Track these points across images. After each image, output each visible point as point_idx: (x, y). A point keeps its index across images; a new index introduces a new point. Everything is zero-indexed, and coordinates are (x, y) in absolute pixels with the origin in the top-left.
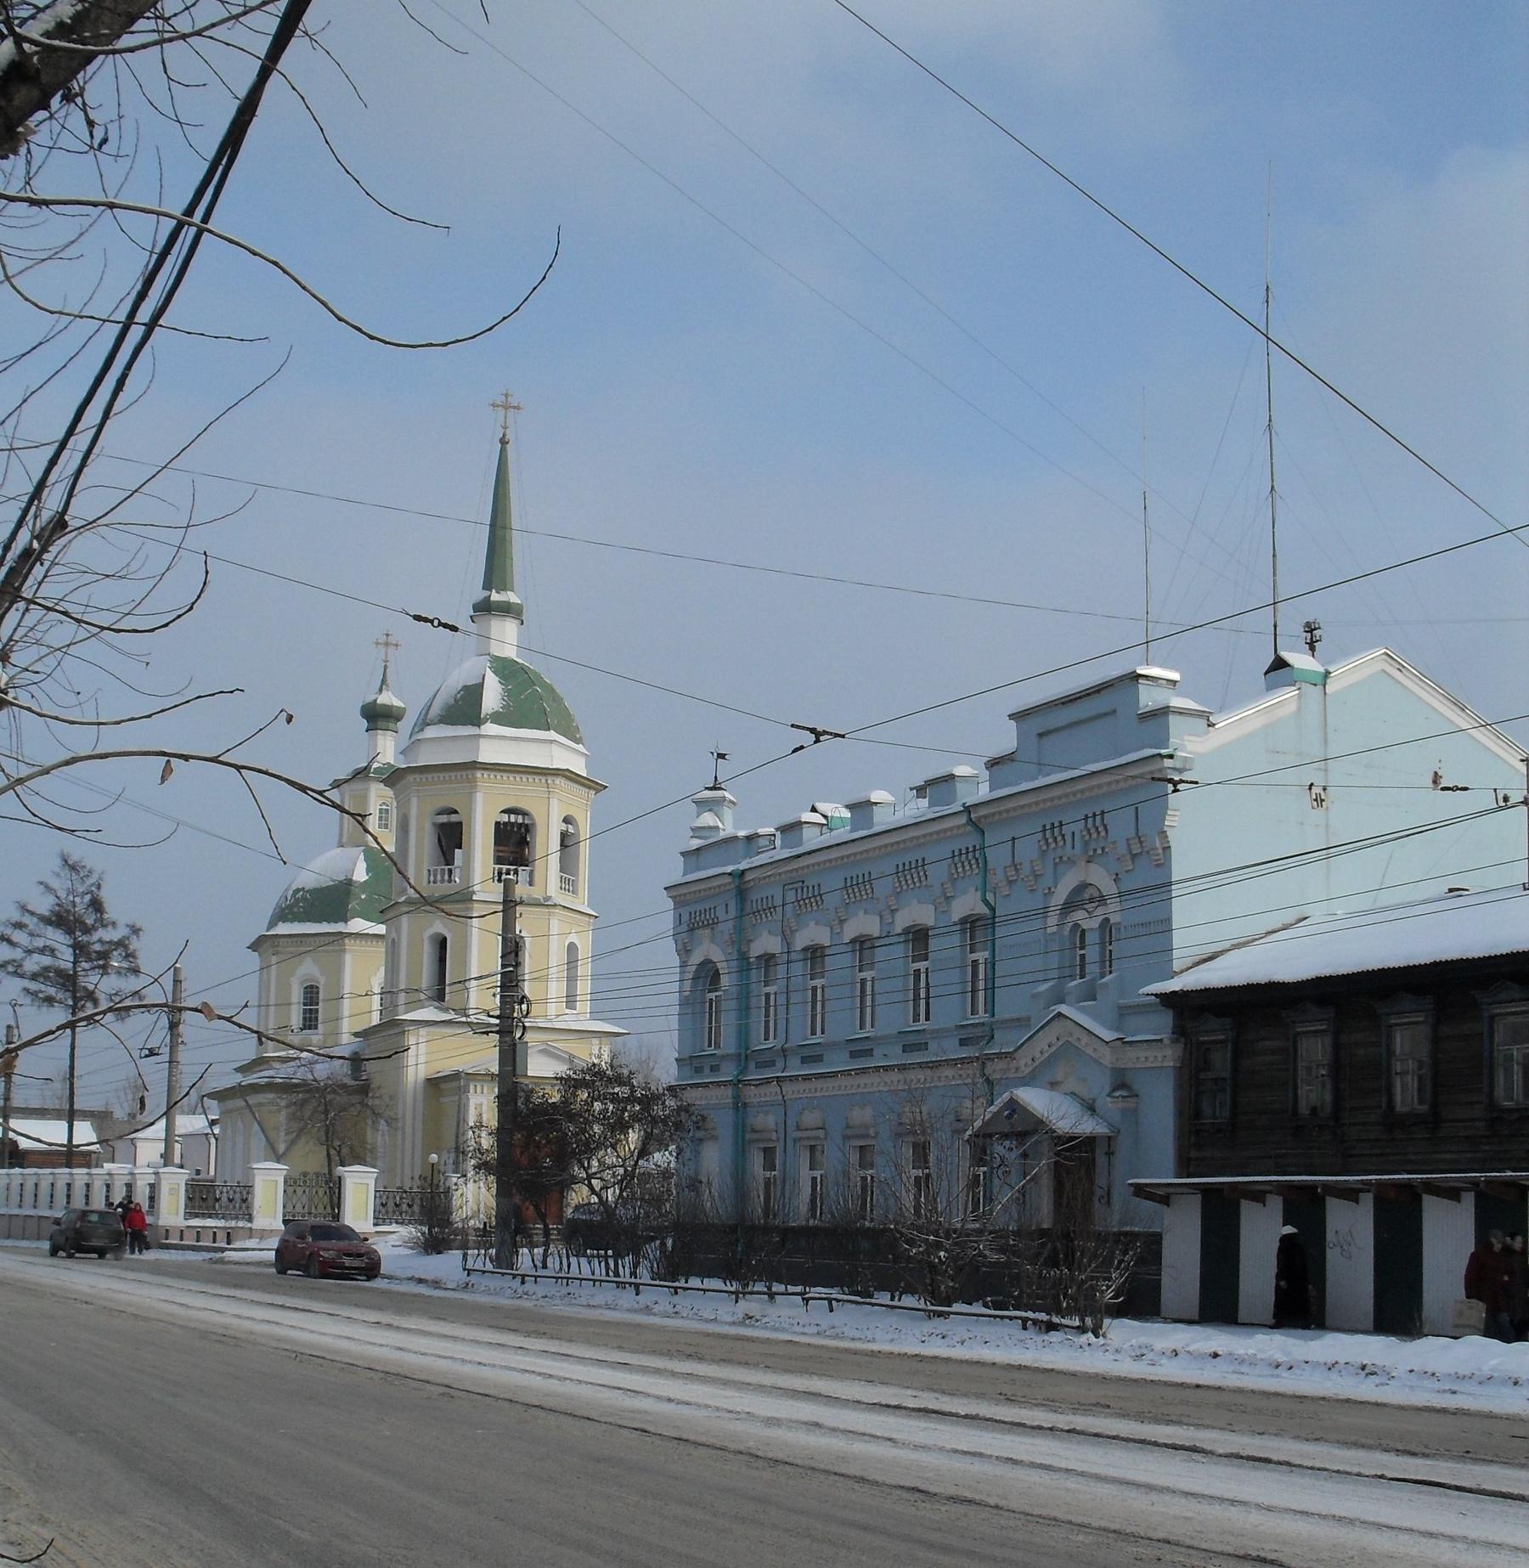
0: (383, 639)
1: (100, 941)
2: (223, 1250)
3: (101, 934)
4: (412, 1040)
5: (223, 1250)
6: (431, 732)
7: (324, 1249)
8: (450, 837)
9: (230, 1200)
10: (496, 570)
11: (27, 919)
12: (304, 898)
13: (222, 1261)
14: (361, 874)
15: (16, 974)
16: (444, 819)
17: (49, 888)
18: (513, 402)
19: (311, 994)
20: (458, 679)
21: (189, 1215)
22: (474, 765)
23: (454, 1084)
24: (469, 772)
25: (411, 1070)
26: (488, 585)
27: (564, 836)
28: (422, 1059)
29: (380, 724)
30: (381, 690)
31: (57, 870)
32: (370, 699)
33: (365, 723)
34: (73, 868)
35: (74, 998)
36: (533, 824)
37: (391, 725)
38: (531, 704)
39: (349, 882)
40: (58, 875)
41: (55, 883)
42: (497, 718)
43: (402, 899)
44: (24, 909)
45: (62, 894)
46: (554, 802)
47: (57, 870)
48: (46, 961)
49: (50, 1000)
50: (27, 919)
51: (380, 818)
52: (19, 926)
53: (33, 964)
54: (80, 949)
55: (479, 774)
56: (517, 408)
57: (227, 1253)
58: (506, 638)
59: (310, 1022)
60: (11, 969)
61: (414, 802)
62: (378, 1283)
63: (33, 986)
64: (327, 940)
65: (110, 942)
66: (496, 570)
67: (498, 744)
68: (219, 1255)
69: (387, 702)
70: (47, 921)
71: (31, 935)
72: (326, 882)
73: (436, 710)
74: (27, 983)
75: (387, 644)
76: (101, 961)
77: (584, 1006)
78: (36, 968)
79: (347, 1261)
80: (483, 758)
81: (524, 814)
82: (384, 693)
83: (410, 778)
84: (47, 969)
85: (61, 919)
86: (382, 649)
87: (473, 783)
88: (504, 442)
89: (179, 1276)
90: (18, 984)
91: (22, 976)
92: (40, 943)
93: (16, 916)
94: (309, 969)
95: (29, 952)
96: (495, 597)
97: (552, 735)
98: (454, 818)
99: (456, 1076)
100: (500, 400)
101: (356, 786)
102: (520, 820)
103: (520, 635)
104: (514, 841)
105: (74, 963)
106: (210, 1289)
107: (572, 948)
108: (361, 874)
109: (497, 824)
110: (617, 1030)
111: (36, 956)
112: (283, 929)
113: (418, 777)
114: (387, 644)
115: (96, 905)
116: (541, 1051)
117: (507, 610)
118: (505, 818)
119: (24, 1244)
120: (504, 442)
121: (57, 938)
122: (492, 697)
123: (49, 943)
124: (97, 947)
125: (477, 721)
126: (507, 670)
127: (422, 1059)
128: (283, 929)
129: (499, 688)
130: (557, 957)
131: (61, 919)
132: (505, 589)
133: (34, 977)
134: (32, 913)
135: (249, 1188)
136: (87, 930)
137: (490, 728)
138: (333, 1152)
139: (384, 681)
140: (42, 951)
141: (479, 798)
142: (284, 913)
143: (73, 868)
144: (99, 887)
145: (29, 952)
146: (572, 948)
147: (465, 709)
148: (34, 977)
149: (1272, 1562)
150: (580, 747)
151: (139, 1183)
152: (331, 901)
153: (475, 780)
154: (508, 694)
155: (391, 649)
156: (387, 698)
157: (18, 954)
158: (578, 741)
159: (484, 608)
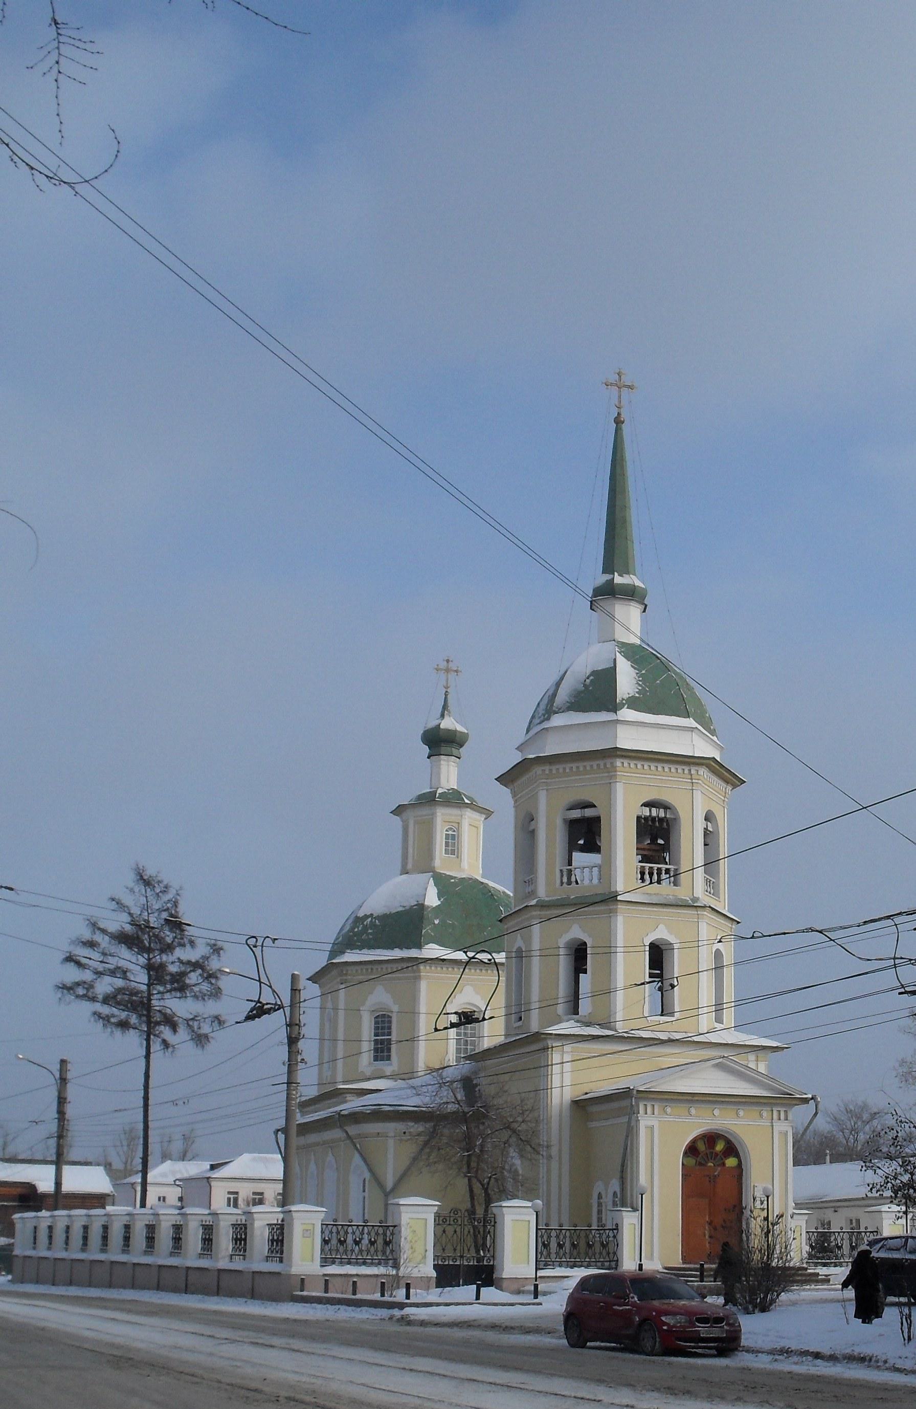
0: (443, 665)
1: (180, 961)
2: (401, 1306)
3: (181, 953)
4: (556, 1057)
5: (401, 1306)
6: (557, 720)
7: (667, 1313)
8: (586, 832)
9: (342, 1242)
10: (615, 552)
11: (99, 938)
12: (373, 925)
13: (405, 1321)
14: (432, 899)
15: (85, 997)
16: (576, 814)
17: (121, 906)
18: (626, 380)
19: (383, 1023)
20: (586, 661)
21: (326, 1261)
22: (615, 752)
23: (624, 1103)
24: (608, 761)
25: (556, 1093)
26: (608, 568)
27: (706, 833)
28: (567, 1081)
29: (443, 749)
30: (442, 716)
31: (131, 884)
32: (432, 724)
33: (426, 750)
34: (147, 883)
35: (149, 1023)
36: (676, 820)
37: (455, 751)
38: (666, 692)
39: (421, 907)
40: (132, 891)
41: (128, 900)
42: (633, 703)
43: (533, 902)
44: (94, 926)
45: (136, 911)
46: (698, 795)
47: (131, 884)
48: (119, 983)
49: (124, 1025)
50: (99, 938)
51: (447, 844)
52: (91, 944)
53: (105, 986)
54: (156, 972)
55: (618, 763)
56: (629, 387)
57: (408, 1310)
58: (629, 621)
59: (382, 1051)
60: (81, 991)
61: (543, 797)
62: (741, 1360)
63: (105, 1010)
64: (395, 966)
65: (189, 963)
66: (615, 552)
67: (636, 730)
68: (397, 1313)
69: (451, 727)
70: (122, 938)
71: (104, 954)
72: (395, 907)
73: (563, 696)
74: (99, 1007)
75: (447, 670)
76: (179, 985)
77: (729, 1016)
78: (109, 990)
79: (703, 1330)
80: (626, 740)
81: (666, 807)
82: (446, 717)
83: (538, 770)
84: (120, 991)
85: (134, 938)
86: (443, 675)
87: (611, 775)
88: (618, 421)
89: (313, 1338)
90: (87, 1007)
91: (93, 999)
92: (113, 962)
93: (87, 935)
94: (380, 996)
95: (99, 974)
96: (618, 580)
97: (690, 722)
98: (589, 813)
99: (626, 1094)
100: (613, 378)
101: (424, 811)
102: (662, 814)
103: (644, 623)
104: (657, 836)
105: (149, 985)
106: (464, 1370)
107: (718, 955)
108: (432, 899)
109: (639, 818)
110: (774, 1044)
111: (107, 979)
112: (350, 956)
113: (547, 768)
114: (447, 670)
115: (176, 925)
116: (717, 1066)
117: (631, 594)
118: (646, 812)
119: (73, 1291)
120: (618, 421)
121: (127, 958)
122: (627, 681)
123: (122, 963)
124: (173, 969)
125: (612, 705)
126: (638, 655)
127: (567, 1081)
128: (350, 956)
129: (632, 672)
130: (706, 961)
131: (134, 938)
132: (628, 573)
133: (106, 1000)
134: (104, 931)
135: (617, 1228)
136: (168, 948)
137: (627, 714)
138: (477, 1188)
139: (445, 707)
140: (113, 973)
141: (620, 790)
142: (339, 948)
143: (147, 883)
144: (176, 904)
145: (99, 974)
146: (718, 955)
147: (598, 693)
148: (106, 1000)
149: (457, 1405)
150: (715, 738)
151: (257, 1224)
152: (404, 927)
153: (614, 768)
154: (644, 679)
155: (452, 676)
156: (448, 723)
157: (88, 976)
158: (713, 732)
159: (608, 592)
